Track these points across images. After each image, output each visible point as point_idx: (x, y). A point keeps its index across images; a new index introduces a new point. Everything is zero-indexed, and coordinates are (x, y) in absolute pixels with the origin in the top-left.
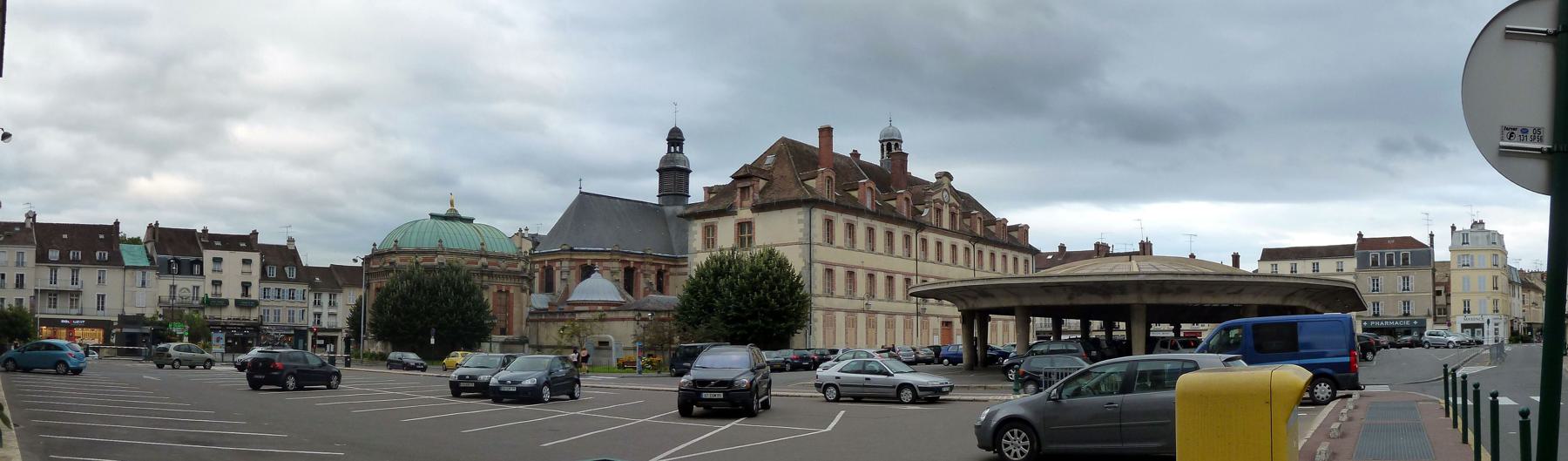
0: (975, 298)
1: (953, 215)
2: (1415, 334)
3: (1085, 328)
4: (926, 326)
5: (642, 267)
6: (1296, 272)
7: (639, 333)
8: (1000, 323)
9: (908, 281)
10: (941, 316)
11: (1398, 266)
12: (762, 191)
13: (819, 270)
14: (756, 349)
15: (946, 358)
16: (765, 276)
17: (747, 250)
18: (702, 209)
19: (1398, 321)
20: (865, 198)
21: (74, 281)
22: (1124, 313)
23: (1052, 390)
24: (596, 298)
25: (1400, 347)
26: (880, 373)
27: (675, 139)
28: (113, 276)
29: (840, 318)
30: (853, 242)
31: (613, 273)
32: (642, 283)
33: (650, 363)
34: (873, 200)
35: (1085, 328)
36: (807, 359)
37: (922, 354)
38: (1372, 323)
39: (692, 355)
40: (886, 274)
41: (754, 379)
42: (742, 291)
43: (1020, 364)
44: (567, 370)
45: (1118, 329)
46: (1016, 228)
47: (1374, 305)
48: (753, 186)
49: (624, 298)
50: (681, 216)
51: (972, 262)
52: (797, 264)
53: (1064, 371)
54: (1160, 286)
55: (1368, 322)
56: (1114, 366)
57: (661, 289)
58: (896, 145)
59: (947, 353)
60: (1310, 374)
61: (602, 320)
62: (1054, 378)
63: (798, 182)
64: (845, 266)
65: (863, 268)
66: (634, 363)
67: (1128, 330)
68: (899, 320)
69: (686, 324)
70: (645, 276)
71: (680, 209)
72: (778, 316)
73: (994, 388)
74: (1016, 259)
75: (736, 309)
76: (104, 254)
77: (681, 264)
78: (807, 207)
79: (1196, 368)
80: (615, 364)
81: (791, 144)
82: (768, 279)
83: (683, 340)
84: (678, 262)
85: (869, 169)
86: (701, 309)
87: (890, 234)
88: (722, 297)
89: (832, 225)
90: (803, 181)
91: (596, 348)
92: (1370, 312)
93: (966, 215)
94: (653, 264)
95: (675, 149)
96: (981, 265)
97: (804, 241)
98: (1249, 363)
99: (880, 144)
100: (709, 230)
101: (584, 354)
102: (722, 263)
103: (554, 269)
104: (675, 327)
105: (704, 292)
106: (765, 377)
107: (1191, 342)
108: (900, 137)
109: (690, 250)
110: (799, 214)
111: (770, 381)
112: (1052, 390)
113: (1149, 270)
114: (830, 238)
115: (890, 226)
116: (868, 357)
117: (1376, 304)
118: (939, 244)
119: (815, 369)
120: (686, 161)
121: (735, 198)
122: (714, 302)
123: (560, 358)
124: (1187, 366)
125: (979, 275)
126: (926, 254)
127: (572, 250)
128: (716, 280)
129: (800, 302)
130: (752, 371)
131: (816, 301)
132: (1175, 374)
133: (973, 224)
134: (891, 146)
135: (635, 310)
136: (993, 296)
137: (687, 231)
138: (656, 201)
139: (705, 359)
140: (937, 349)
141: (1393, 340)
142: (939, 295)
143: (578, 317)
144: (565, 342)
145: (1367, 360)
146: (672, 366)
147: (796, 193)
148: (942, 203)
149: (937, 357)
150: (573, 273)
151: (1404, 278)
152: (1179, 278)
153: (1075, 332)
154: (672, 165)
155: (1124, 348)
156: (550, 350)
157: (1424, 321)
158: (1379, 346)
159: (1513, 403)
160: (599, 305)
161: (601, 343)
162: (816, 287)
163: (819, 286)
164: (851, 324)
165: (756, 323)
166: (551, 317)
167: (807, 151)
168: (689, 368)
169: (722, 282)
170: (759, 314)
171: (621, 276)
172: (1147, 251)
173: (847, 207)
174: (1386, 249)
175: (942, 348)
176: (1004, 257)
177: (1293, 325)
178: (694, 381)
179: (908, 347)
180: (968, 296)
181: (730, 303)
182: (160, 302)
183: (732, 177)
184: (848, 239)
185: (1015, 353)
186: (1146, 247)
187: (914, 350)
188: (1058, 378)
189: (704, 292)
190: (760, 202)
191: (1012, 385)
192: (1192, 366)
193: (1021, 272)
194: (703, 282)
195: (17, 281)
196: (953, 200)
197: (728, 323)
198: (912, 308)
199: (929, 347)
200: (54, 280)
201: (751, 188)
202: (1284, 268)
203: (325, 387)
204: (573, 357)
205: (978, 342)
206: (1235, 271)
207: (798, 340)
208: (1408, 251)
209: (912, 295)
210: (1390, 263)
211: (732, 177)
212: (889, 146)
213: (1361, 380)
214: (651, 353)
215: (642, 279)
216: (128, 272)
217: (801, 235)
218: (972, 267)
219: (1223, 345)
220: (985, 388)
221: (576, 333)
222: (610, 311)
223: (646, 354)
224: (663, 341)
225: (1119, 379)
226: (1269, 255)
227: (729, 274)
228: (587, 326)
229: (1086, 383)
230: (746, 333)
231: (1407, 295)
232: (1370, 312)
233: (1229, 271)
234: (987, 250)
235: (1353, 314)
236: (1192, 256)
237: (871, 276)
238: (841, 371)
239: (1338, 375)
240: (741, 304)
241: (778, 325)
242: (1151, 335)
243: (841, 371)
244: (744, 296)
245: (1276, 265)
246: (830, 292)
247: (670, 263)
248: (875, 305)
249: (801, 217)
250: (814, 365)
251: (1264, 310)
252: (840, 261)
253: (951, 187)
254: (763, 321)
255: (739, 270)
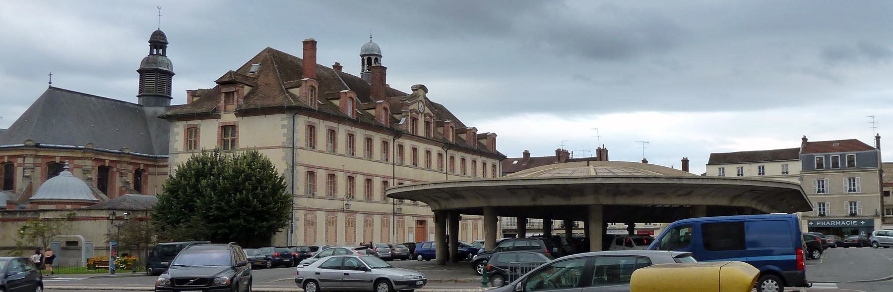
0: (447, 199)
1: (427, 124)
2: (863, 234)
3: (548, 227)
4: (401, 225)
5: (118, 166)
6: (742, 175)
7: (112, 232)
8: (470, 222)
9: (385, 183)
10: (416, 216)
11: (843, 167)
12: (246, 96)
13: (301, 172)
14: (237, 247)
15: (420, 254)
16: (248, 178)
17: (230, 152)
18: (184, 111)
19: (845, 221)
20: (346, 106)
22: (582, 213)
23: (518, 283)
24: (64, 197)
25: (847, 246)
26: (358, 268)
27: (158, 42)
29: (321, 217)
30: (334, 147)
31: (85, 171)
32: (118, 182)
33: (125, 262)
34: (353, 109)
35: (548, 227)
36: (288, 256)
37: (398, 251)
38: (818, 223)
39: (171, 254)
40: (365, 177)
41: (235, 276)
42: (225, 191)
43: (488, 260)
44: (28, 272)
45: (577, 228)
46: (484, 136)
47: (820, 206)
48: (237, 91)
49: (97, 197)
50: (162, 117)
51: (445, 166)
52: (280, 166)
53: (528, 266)
54: (616, 189)
55: (815, 222)
56: (574, 261)
57: (138, 188)
58: (376, 60)
59: (421, 249)
60: (757, 271)
61: (71, 219)
62: (519, 272)
63: (282, 90)
64: (326, 169)
65: (343, 171)
66: (107, 263)
67: (587, 228)
68: (377, 219)
69: (165, 223)
70: (122, 175)
71: (161, 110)
72: (260, 216)
73: (464, 282)
74: (484, 164)
75: (218, 209)
77: (161, 164)
78: (292, 114)
79: (649, 264)
80: (84, 264)
81: (276, 55)
82: (250, 180)
83: (160, 238)
84: (158, 162)
85: (350, 80)
86: (181, 208)
87: (369, 140)
88: (203, 196)
89: (314, 131)
90: (287, 89)
91: (63, 249)
92: (816, 212)
93: (440, 124)
94: (131, 163)
95: (158, 52)
96: (453, 169)
97: (287, 145)
98: (699, 259)
99: (361, 58)
100: (191, 132)
101: (48, 254)
102: (204, 164)
103: (15, 165)
104: (153, 227)
105: (185, 192)
106: (246, 274)
107: (644, 240)
108: (380, 53)
109: (171, 150)
110: (282, 119)
111: (251, 277)
112: (518, 283)
113: (605, 174)
114: (312, 143)
115: (369, 133)
116: (347, 254)
117: (822, 205)
118: (415, 150)
119: (296, 265)
120: (169, 64)
121: (219, 102)
122: (195, 202)
123: (19, 260)
124: (640, 261)
125: (451, 178)
126: (402, 159)
127: (37, 146)
128: (197, 180)
129: (282, 203)
130: (233, 268)
131: (298, 202)
132: (630, 269)
133: (445, 133)
134: (371, 60)
135: (109, 209)
136: (463, 198)
137: (169, 132)
138: (136, 101)
139: (183, 257)
140: (411, 246)
141: (839, 239)
142: (414, 196)
143: (42, 216)
144: (25, 242)
145: (813, 258)
146: (148, 266)
147: (279, 101)
148: (418, 113)
149: (411, 254)
150: (38, 170)
151: (850, 180)
152: (633, 181)
153: (538, 230)
154: (154, 67)
155: (583, 245)
156: (8, 251)
157: (872, 221)
158: (826, 245)
160: (68, 203)
161: (69, 243)
162: (298, 189)
163: (300, 187)
164: (331, 223)
165: (238, 222)
166: (10, 216)
167: (291, 62)
168: (167, 267)
169: (204, 182)
170: (241, 214)
171: (94, 175)
172: (604, 157)
173: (329, 115)
174: (831, 152)
175: (417, 245)
176: (474, 162)
177: (740, 225)
178: (172, 280)
179: (385, 245)
180: (440, 197)
181: (212, 203)
183: (217, 82)
184: (349, 148)
185: (483, 249)
186: (602, 154)
187: (391, 247)
188: (522, 272)
189: (185, 192)
190: (244, 107)
191: (480, 278)
192: (645, 262)
193: (489, 176)
194: (183, 182)
196: (427, 110)
197: (209, 222)
198: (389, 208)
199: (404, 244)
201: (235, 93)
202: (731, 171)
204: (36, 258)
205: (449, 239)
206: (684, 174)
207: (279, 238)
208: (853, 153)
209: (389, 196)
210: (835, 165)
211: (217, 82)
212: (369, 60)
213: (808, 277)
214: (127, 252)
215: (117, 177)
217: (284, 139)
218: (445, 171)
219: (674, 243)
220: (456, 281)
221: (39, 233)
222: (80, 210)
223: (120, 253)
224: (139, 240)
225: (578, 273)
226: (717, 159)
227: (211, 174)
228: (54, 225)
229: (547, 277)
230: (228, 232)
231: (853, 196)
232: (816, 212)
233: (679, 175)
234: (458, 156)
235: (799, 214)
236: (645, 161)
237: (351, 179)
238: (321, 267)
239: (785, 272)
240: (223, 204)
241: (260, 224)
242: (608, 233)
243: (321, 267)
244: (226, 196)
245: (723, 169)
246: (311, 192)
247: (149, 163)
248: (354, 205)
249: (285, 122)
250: (295, 261)
251: (712, 210)
252: (340, 168)
253: (426, 98)
254: (245, 220)
255: (221, 171)
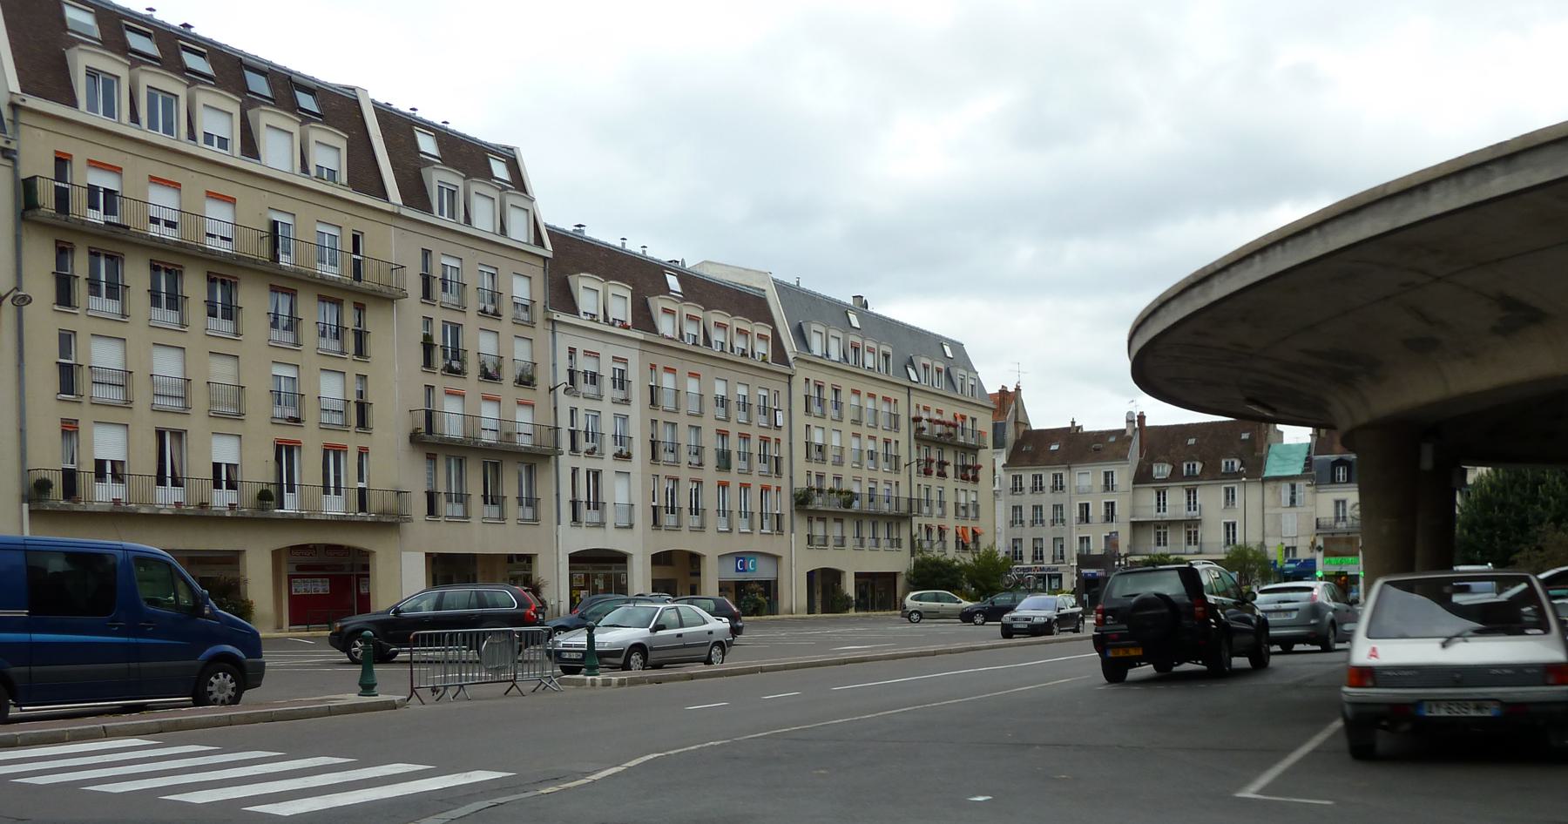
21: (1191, 503)
28: (1250, 496)
76: (1233, 463)
159: (1481, 626)
182: (1318, 527)
195: (1081, 513)
200: (1161, 504)
203: (1319, 648)
216: (1269, 487)
